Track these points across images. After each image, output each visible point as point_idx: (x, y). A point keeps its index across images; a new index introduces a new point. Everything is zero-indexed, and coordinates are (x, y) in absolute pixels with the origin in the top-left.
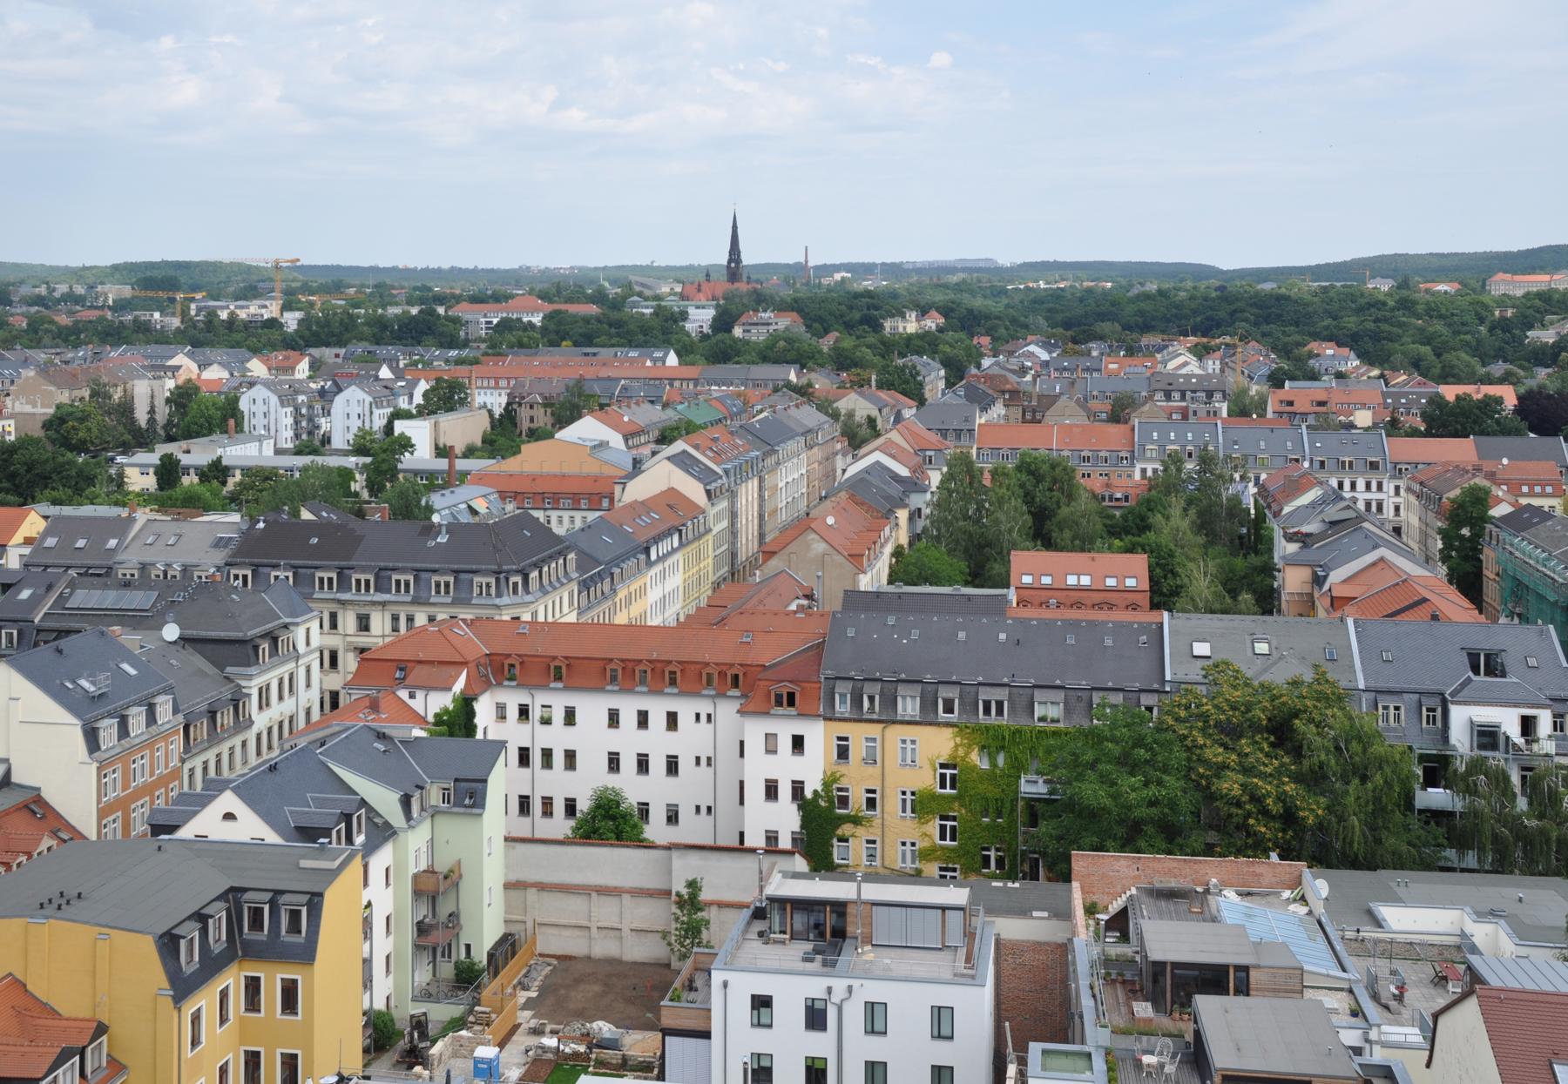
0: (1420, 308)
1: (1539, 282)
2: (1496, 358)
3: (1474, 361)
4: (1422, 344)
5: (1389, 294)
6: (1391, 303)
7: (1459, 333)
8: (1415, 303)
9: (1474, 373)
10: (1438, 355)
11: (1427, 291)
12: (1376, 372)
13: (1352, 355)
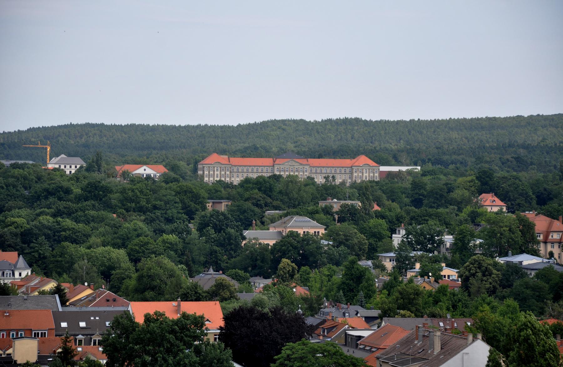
0: (115, 198)
1: (258, 168)
2: (206, 265)
3: (180, 269)
4: (116, 246)
5: (76, 178)
6: (77, 190)
7: (162, 231)
8: (107, 190)
9: (178, 285)
10: (135, 260)
11: (125, 175)
12: (51, 285)
13: (21, 261)
